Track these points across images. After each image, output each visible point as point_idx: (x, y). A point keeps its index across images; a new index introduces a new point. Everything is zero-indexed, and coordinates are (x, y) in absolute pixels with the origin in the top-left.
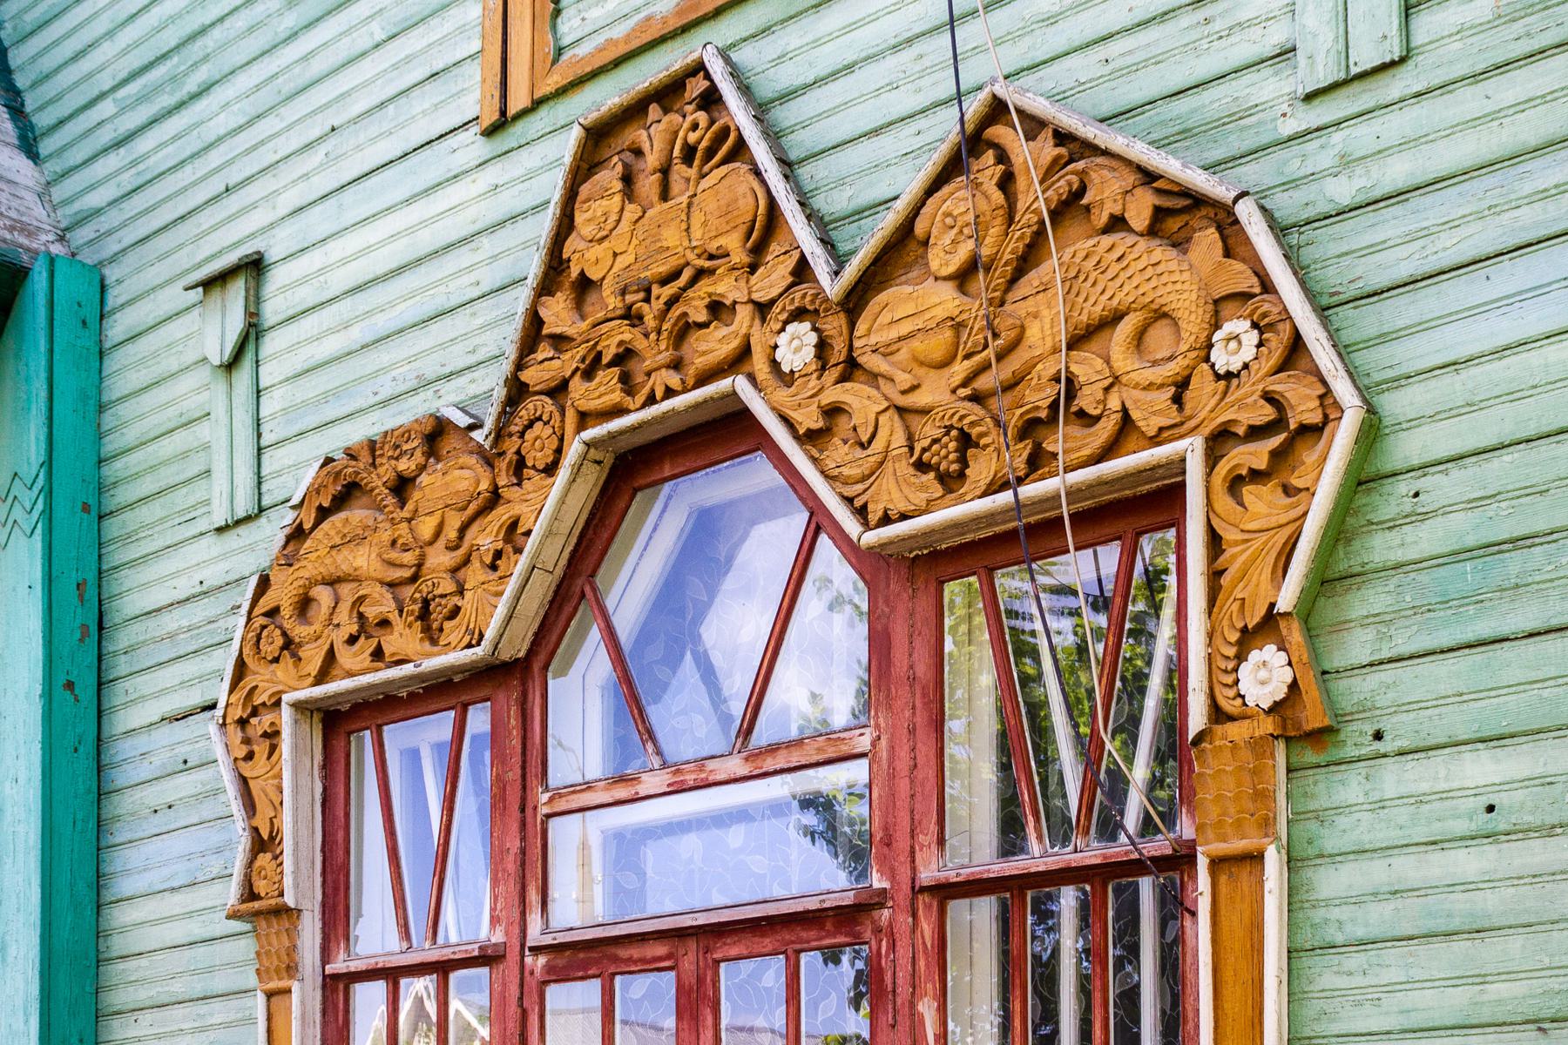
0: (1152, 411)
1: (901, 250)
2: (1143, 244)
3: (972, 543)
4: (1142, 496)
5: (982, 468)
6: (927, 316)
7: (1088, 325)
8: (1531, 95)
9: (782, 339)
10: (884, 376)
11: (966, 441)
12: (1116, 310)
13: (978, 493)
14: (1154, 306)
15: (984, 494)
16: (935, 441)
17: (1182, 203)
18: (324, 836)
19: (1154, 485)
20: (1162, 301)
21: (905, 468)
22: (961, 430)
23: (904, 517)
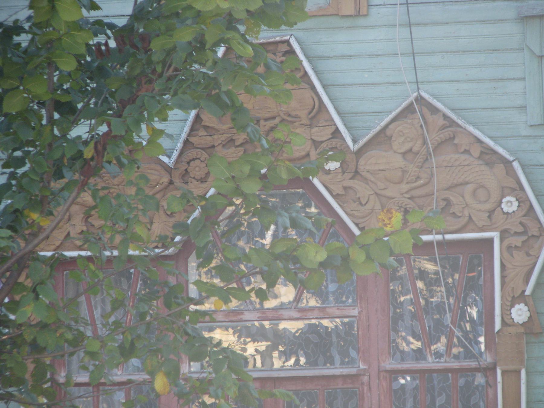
1: (382, 138)
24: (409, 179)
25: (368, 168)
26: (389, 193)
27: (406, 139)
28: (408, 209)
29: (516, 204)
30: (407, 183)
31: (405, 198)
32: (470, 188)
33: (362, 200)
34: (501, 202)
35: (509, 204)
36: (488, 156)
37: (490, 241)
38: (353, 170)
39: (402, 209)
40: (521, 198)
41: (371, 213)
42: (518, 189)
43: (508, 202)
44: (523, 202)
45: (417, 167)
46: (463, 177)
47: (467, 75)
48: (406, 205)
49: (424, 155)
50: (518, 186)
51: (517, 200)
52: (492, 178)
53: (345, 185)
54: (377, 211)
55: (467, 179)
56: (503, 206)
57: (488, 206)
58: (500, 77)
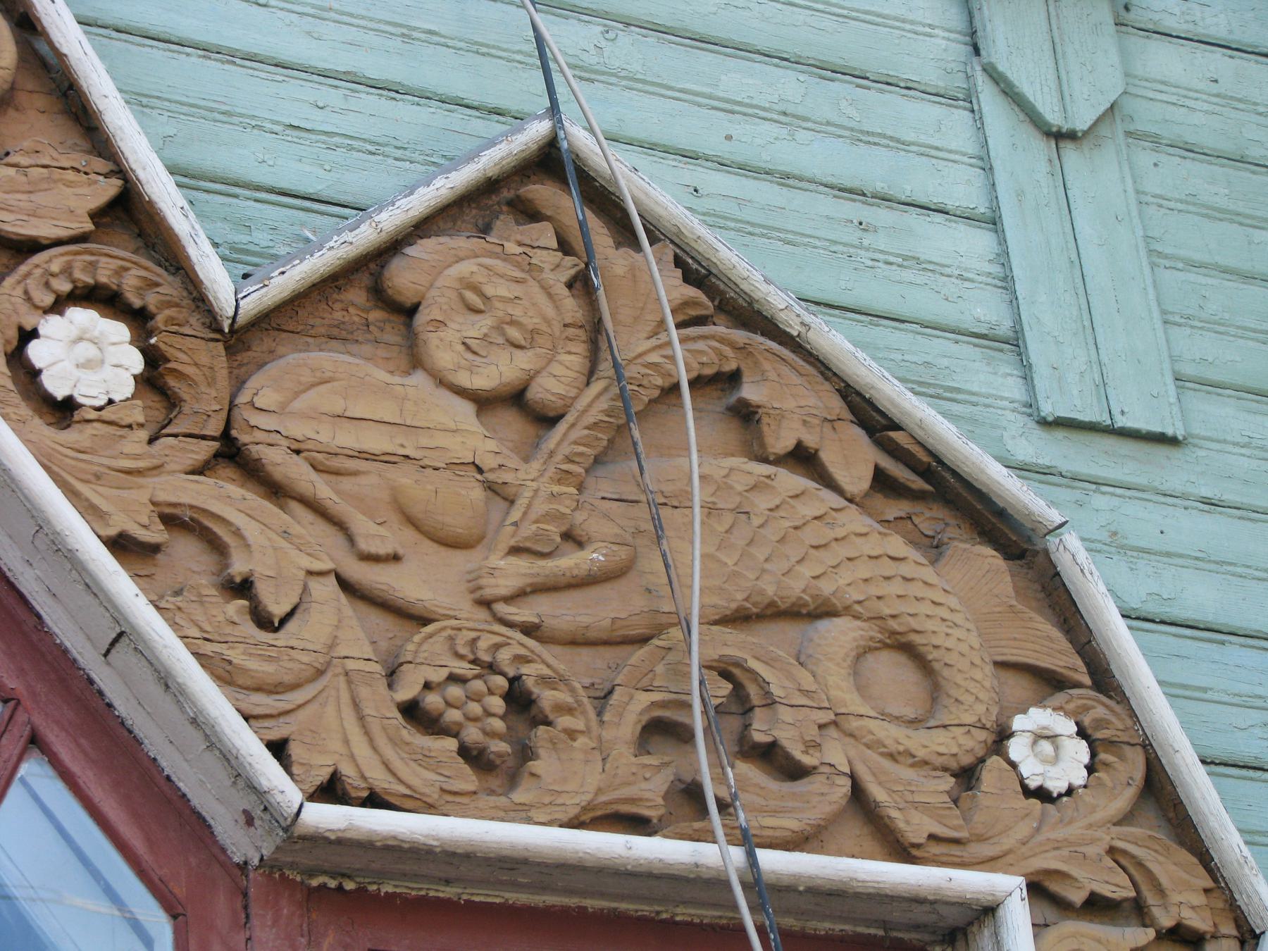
0: (916, 803)
1: (369, 294)
2: (855, 520)
3: (472, 908)
4: (816, 938)
5: (566, 769)
6: (425, 441)
7: (772, 604)
8: (867, 146)
9: (51, 326)
10: (877, 649)
11: (519, 700)
12: (826, 601)
13: (564, 817)
14: (893, 625)
15: (575, 823)
16: (453, 678)
17: (918, 483)
18: (689, 927)
19: (838, 927)
20: (914, 624)
21: (382, 705)
22: (514, 681)
23: (374, 800)
24: (528, 529)
25: (298, 429)
26: (404, 583)
27: (499, 328)
28: (530, 683)
29: (1079, 751)
30: (516, 551)
31: (510, 625)
32: (838, 636)
33: (264, 590)
34: (1003, 735)
35: (1046, 747)
36: (927, 488)
37: (988, 911)
38: (214, 427)
39: (500, 682)
40: (1100, 723)
41: (320, 673)
42: (1087, 680)
43: (1040, 736)
44: (1111, 744)
45: (563, 477)
46: (807, 571)
47: (729, 138)
48: (520, 659)
49: (595, 426)
50: (1079, 663)
51: (1082, 733)
52: (960, 598)
53: (162, 496)
54: (351, 665)
55: (826, 587)
56: (1017, 749)
57: (955, 744)
58: (880, 186)
